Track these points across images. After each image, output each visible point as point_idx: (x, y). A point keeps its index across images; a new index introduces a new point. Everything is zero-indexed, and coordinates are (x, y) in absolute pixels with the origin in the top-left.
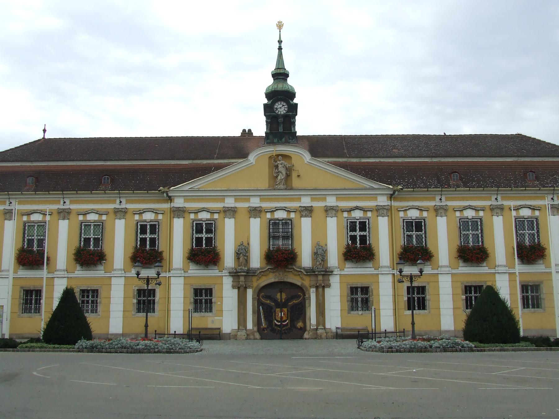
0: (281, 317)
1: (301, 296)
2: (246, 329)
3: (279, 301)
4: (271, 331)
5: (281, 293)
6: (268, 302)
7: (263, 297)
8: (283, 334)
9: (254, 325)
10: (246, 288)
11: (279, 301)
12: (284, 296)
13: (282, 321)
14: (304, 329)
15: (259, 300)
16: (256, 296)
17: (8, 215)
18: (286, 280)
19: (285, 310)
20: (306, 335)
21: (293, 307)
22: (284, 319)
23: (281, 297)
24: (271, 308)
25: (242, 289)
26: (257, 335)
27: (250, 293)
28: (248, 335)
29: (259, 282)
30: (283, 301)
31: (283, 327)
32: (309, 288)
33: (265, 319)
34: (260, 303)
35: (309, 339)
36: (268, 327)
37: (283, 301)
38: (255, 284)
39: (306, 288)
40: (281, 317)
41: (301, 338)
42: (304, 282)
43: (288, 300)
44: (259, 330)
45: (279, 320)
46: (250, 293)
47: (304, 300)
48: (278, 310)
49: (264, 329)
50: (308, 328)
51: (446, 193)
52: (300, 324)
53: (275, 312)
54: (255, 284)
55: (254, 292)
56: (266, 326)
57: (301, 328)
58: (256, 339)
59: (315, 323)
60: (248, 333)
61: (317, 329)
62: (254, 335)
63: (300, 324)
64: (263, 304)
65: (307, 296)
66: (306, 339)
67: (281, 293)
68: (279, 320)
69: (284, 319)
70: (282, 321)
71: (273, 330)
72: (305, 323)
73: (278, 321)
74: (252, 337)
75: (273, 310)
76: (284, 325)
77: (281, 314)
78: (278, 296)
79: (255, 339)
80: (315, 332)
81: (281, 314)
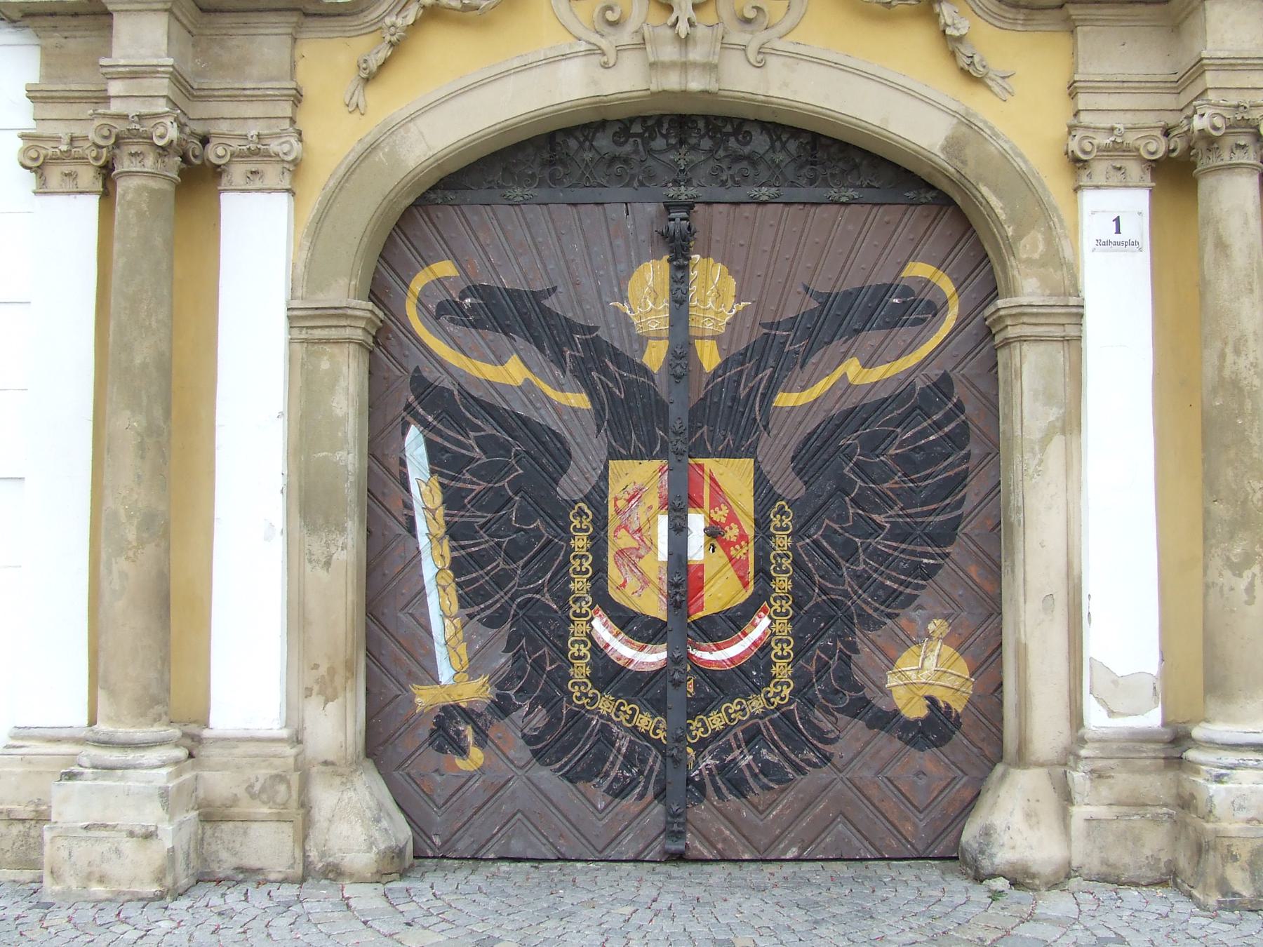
0: (683, 581)
1: (935, 309)
2: (194, 746)
3: (655, 357)
4: (544, 748)
5: (678, 249)
6: (514, 372)
7: (445, 311)
8: (697, 788)
9: (307, 682)
10: (198, 176)
11: (655, 357)
12: (716, 297)
13: (684, 620)
14: (971, 737)
15: (383, 344)
16: (343, 291)
17: (1034, 820)
18: (752, 80)
19: (734, 477)
20: (1015, 822)
21: (820, 448)
22: (723, 590)
23: (678, 305)
24: (548, 450)
25: (142, 179)
26: (356, 819)
27: (259, 247)
28: (211, 815)
29: (387, 103)
30: (709, 357)
31: (702, 706)
32: (1054, 184)
33: (470, 597)
34: (401, 391)
35: (1062, 877)
36: (502, 707)
37: (709, 357)
38: (332, 137)
39: (1023, 185)
40: (683, 581)
41: (944, 845)
42: (980, 104)
43: (771, 351)
44: (378, 745)
45: (653, 605)
46: (259, 247)
47: (985, 341)
48: (635, 480)
49: (447, 727)
50: (1045, 728)
51: (1033, 320)
52: (923, 672)
53: (597, 498)
54: (332, 137)
55: (316, 234)
56: (475, 692)
57: (937, 726)
58: (334, 873)
59: (1151, 664)
60: (220, 783)
61: (1174, 745)
62: (303, 819)
63: (923, 672)
64: (441, 404)
65: (1028, 288)
66: (1020, 879)
67: (678, 249)
68: (653, 605)
69: (723, 590)
70: (684, 620)
71: (568, 743)
72: (987, 652)
73: (626, 620)
74: (268, 845)
75: (571, 485)
76: (706, 674)
77: (670, 539)
78: (645, 295)
79: (318, 872)
80: (1156, 785)
81: (670, 539)
